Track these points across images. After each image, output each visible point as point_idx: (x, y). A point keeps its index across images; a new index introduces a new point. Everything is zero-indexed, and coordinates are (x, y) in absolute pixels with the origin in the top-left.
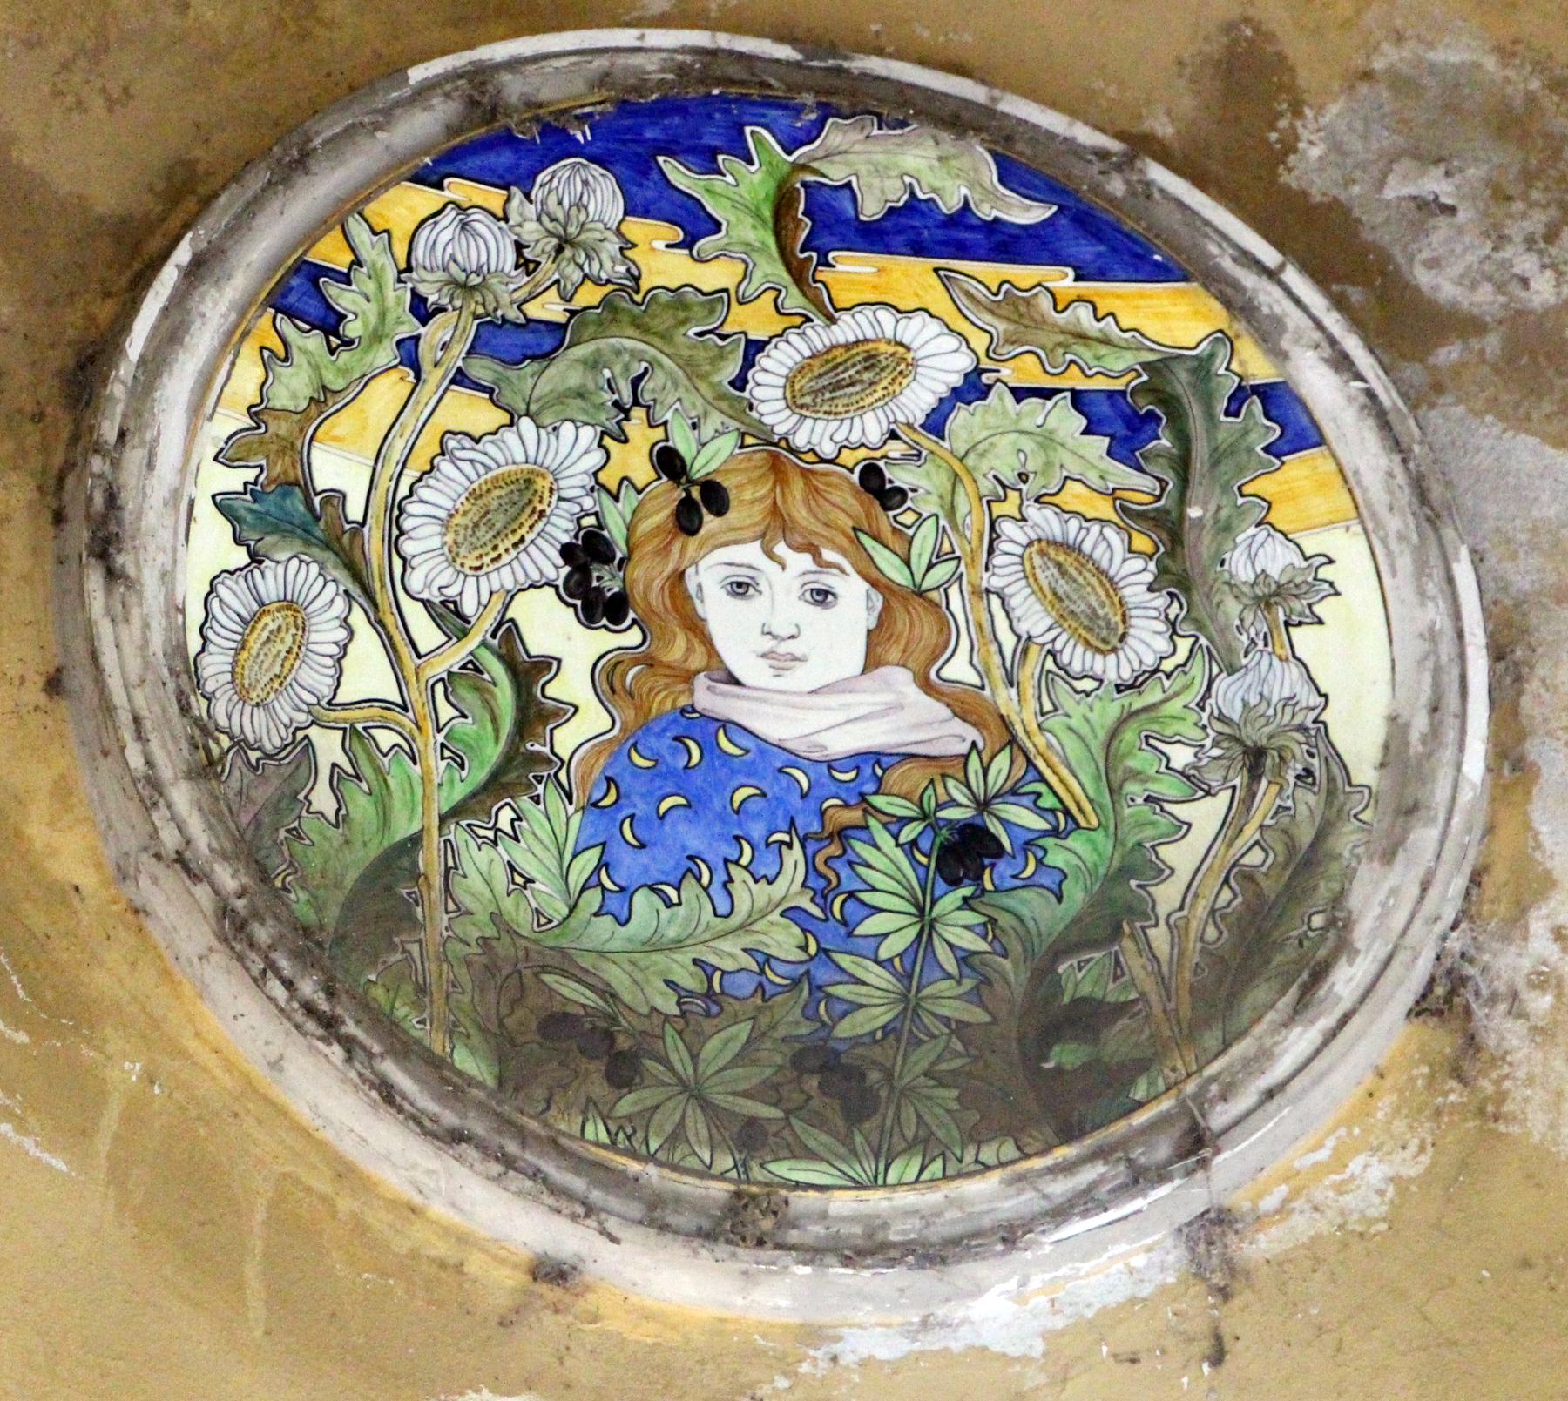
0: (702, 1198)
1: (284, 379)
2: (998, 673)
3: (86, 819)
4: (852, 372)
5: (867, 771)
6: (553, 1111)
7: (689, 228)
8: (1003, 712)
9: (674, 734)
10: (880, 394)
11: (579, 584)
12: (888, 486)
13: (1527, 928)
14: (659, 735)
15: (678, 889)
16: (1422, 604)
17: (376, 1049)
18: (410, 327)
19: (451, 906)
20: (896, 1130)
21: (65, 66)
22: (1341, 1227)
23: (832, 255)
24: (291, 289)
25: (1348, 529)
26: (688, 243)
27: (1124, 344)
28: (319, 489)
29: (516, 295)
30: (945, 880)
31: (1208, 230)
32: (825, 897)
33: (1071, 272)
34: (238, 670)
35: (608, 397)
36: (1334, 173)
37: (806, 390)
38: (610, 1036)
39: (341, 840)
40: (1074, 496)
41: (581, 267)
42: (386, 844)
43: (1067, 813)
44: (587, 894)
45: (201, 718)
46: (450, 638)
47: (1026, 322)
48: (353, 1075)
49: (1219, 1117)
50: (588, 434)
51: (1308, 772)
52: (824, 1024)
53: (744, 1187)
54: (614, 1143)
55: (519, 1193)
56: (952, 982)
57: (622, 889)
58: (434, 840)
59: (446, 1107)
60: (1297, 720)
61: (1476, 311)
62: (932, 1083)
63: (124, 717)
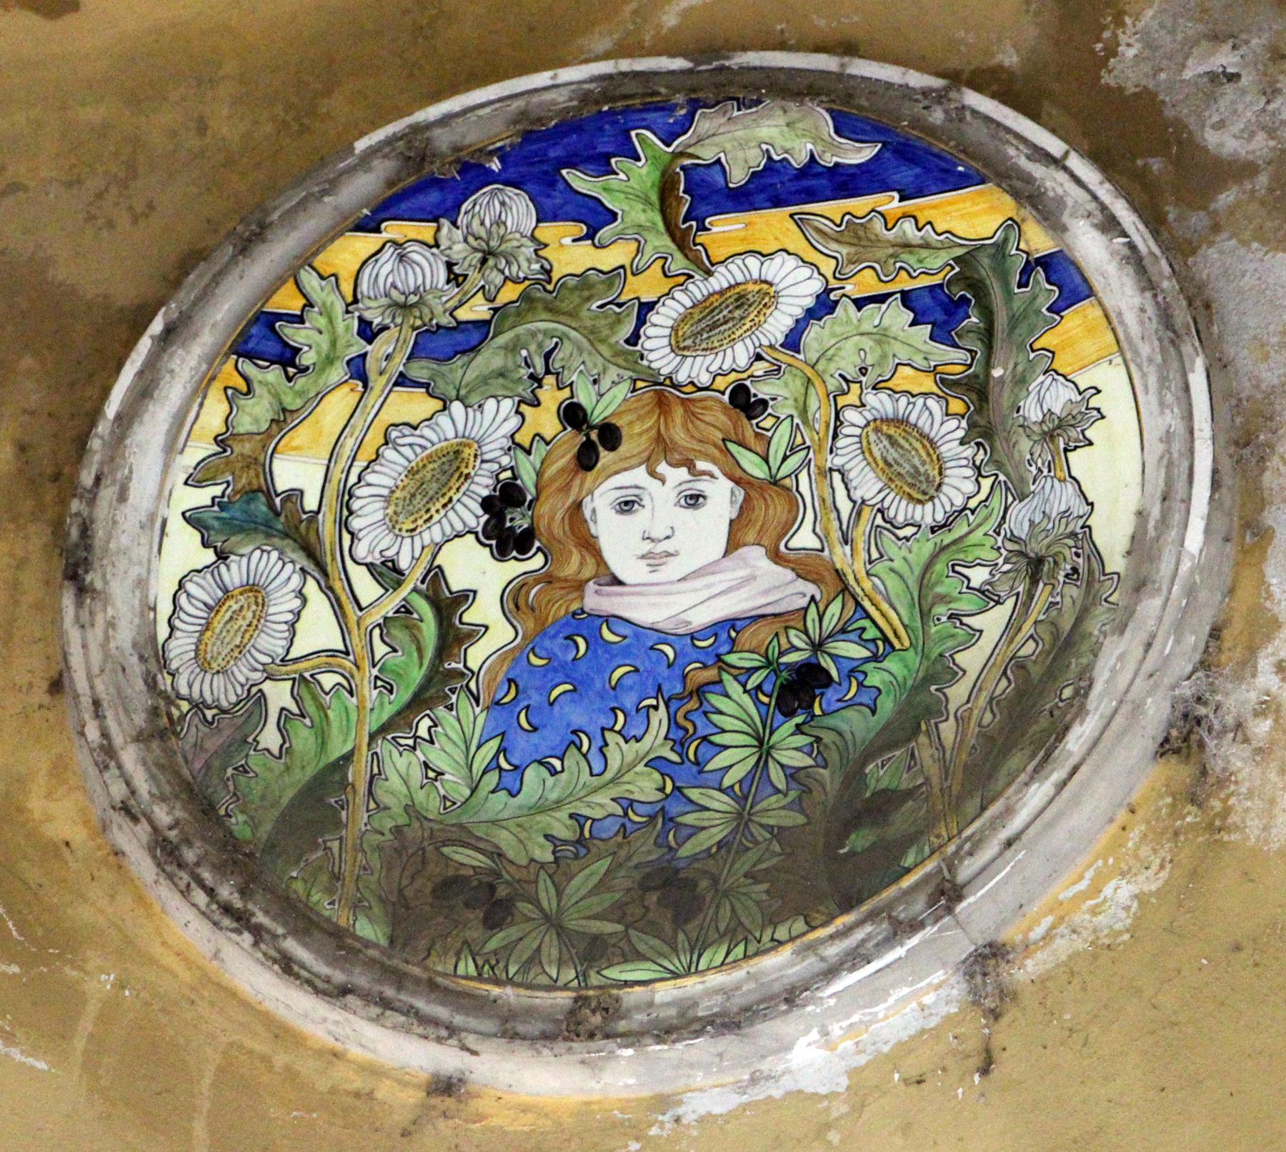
0: (552, 1006)
1: (248, 410)
2: (836, 535)
3: (78, 788)
4: (725, 312)
5: (724, 636)
6: (433, 958)
7: (590, 222)
8: (838, 566)
9: (566, 634)
10: (748, 325)
11: (495, 527)
12: (753, 400)
13: (1255, 667)
14: (554, 637)
15: (562, 760)
16: (1162, 413)
17: (280, 931)
18: (359, 346)
19: (372, 805)
20: (713, 924)
21: (99, 196)
22: (1092, 943)
23: (708, 220)
24: (251, 337)
25: (1111, 362)
26: (590, 236)
27: (939, 245)
28: (280, 490)
29: (448, 305)
30: (781, 712)
31: (1009, 137)
32: (682, 745)
33: (896, 195)
34: (202, 647)
35: (524, 372)
36: (1146, 68)
37: (688, 333)
38: (492, 888)
39: (282, 768)
40: (905, 378)
41: (502, 272)
42: (321, 765)
43: (886, 640)
44: (486, 777)
45: (165, 691)
46: (387, 590)
47: (864, 243)
48: (260, 955)
49: (966, 870)
50: (507, 405)
51: (1075, 570)
52: (670, 848)
53: (584, 992)
54: (480, 975)
55: (394, 1028)
56: (780, 796)
57: (516, 767)
58: (364, 754)
59: (335, 968)
60: (1069, 530)
61: (1251, 157)
62: (750, 881)
63: (86, 701)
